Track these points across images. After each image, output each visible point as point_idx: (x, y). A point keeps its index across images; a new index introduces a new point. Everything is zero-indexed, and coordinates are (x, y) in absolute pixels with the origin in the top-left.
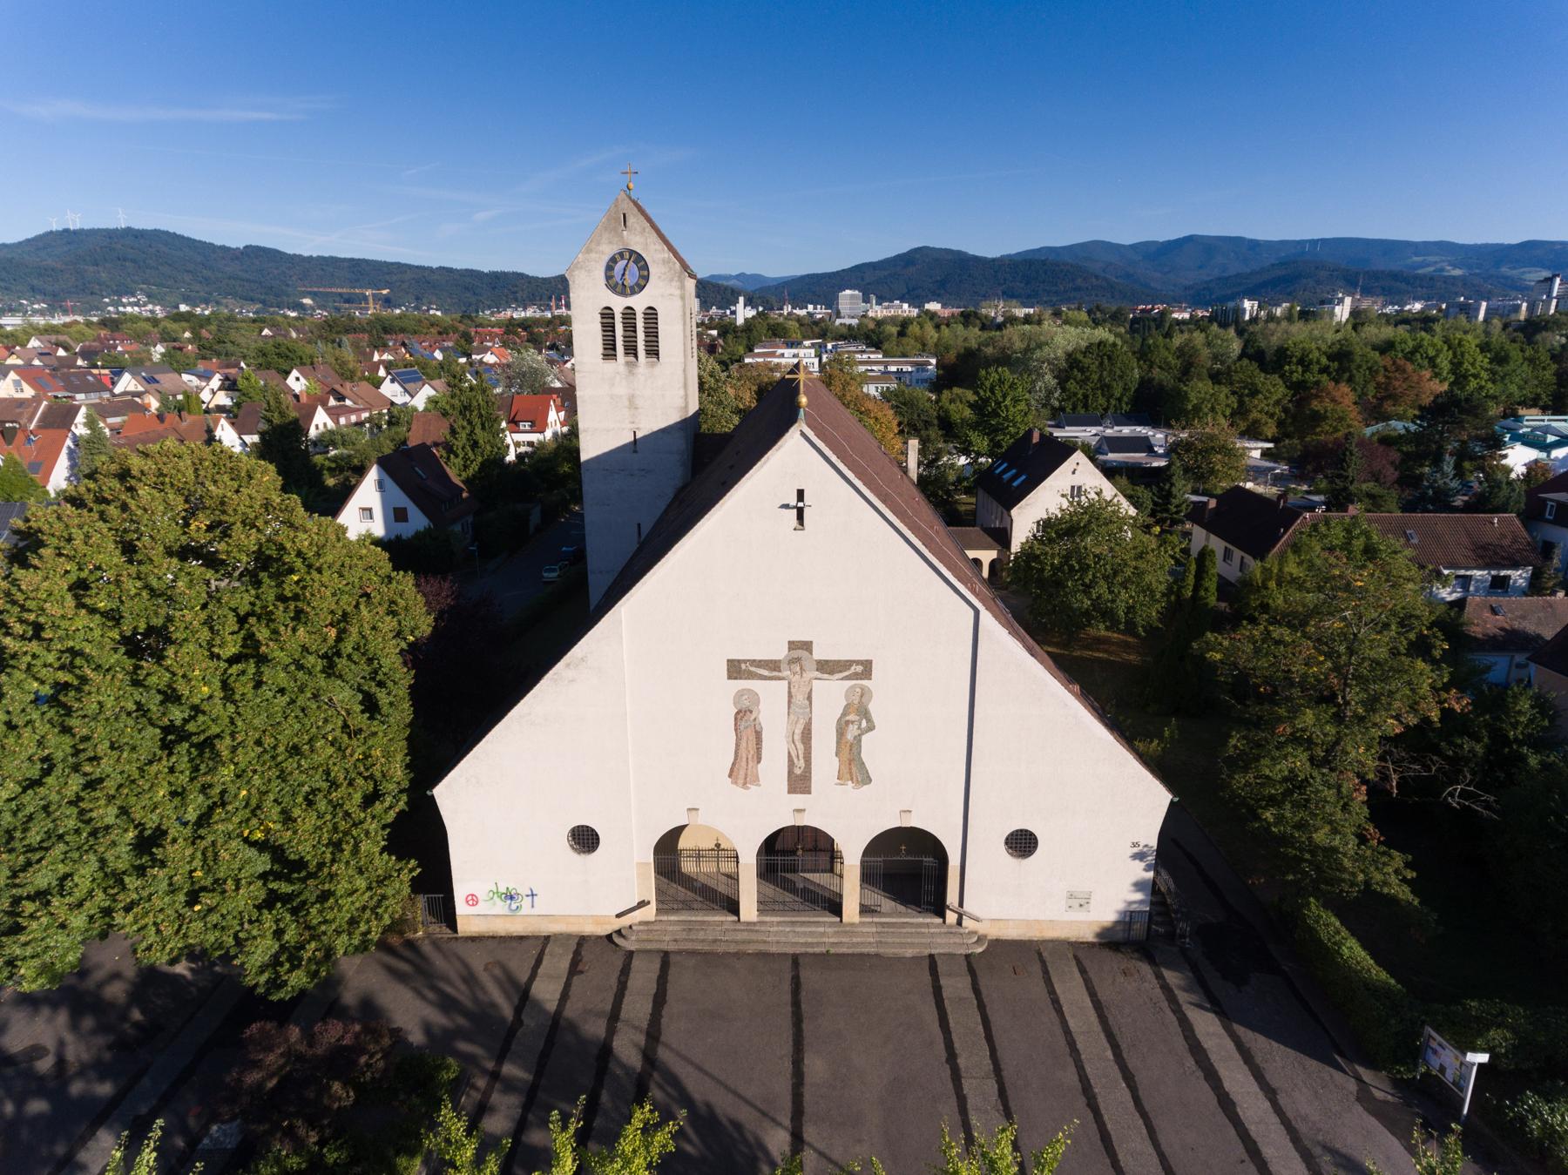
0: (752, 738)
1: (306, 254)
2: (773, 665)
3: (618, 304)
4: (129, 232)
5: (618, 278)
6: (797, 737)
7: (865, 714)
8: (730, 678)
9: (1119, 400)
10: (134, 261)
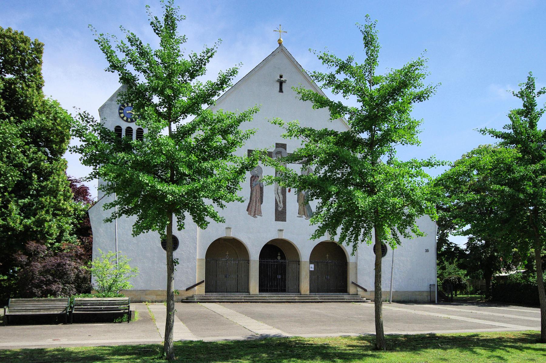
0: (259, 190)
6: (279, 191)
8: (276, 220)
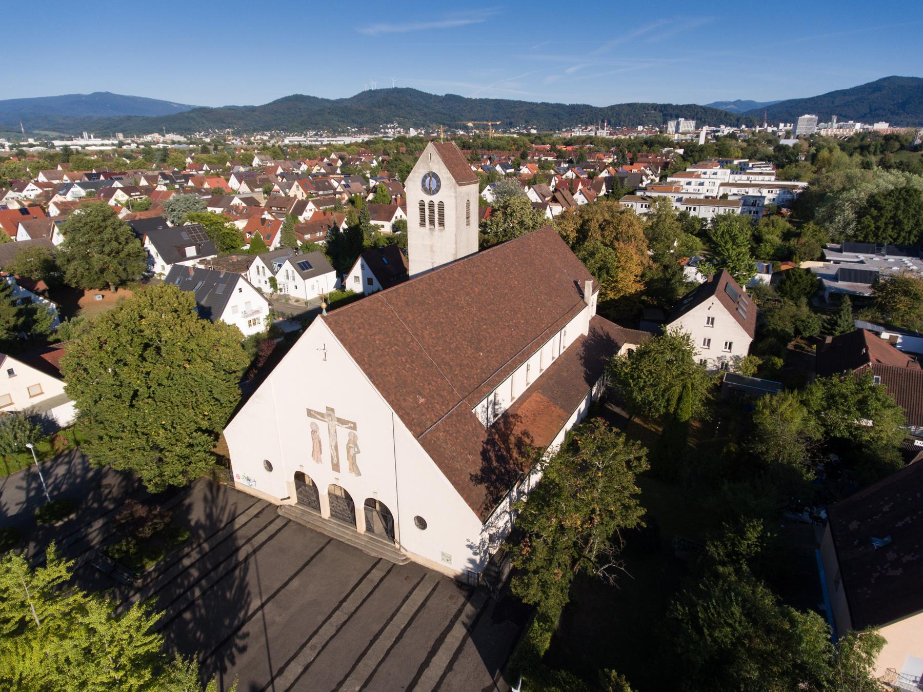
1: (474, 98)
2: (322, 415)
3: (427, 199)
4: (396, 91)
5: (427, 186)
7: (356, 445)
9: (910, 233)
10: (395, 105)
